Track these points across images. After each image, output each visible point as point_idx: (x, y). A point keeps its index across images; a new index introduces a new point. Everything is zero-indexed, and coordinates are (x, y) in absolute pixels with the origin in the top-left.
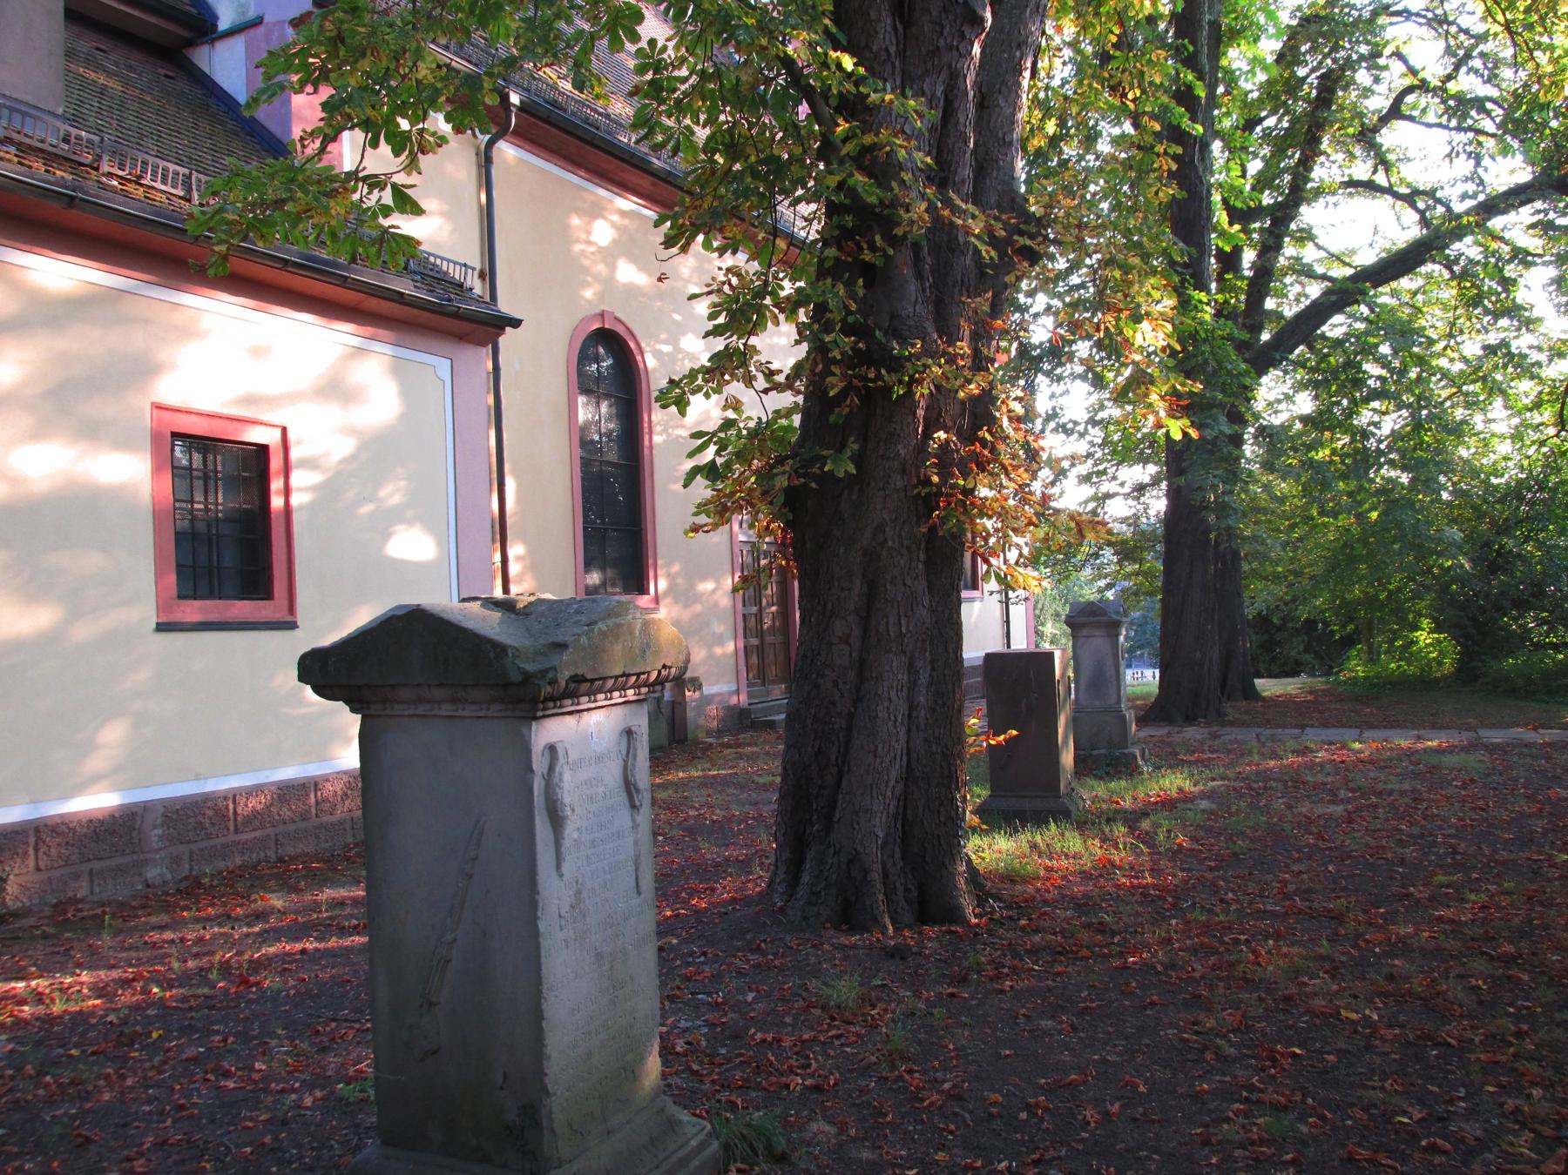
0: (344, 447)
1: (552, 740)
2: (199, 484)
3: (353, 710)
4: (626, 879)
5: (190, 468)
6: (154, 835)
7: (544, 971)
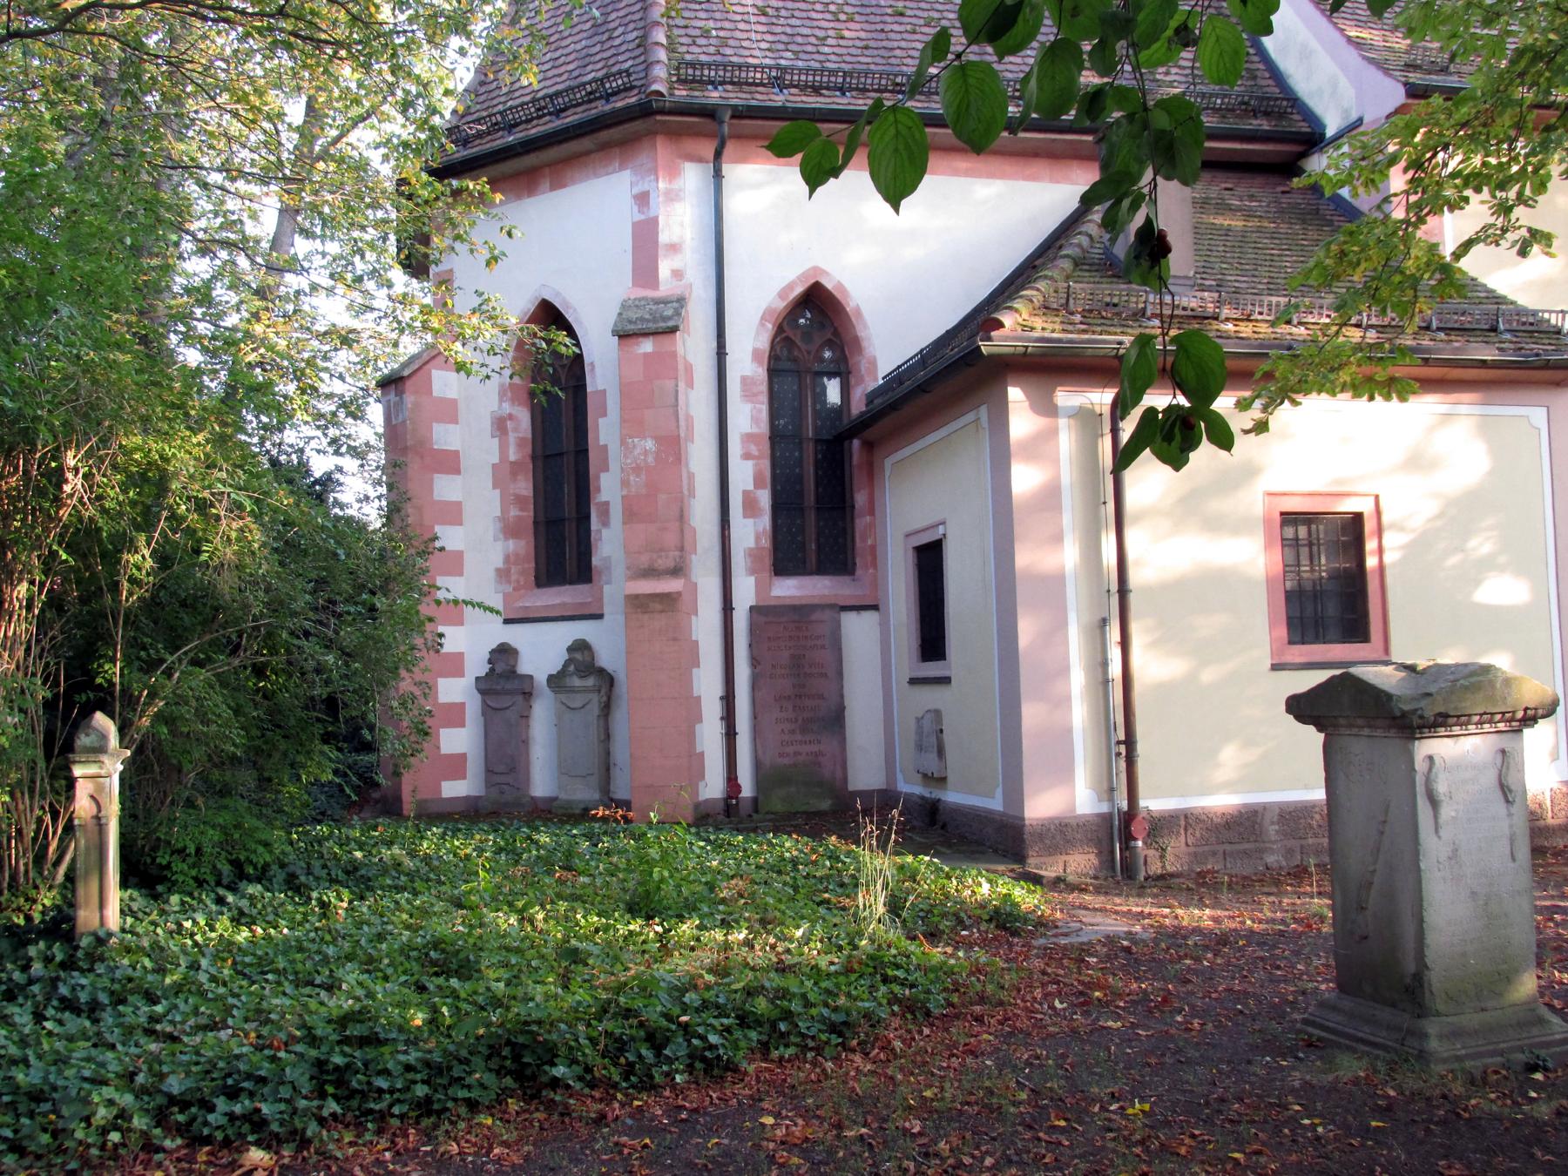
0: (1431, 508)
1: (1430, 752)
2: (1304, 551)
3: (1320, 730)
4: (1503, 847)
5: (1297, 539)
6: (1272, 830)
7: (1424, 894)
